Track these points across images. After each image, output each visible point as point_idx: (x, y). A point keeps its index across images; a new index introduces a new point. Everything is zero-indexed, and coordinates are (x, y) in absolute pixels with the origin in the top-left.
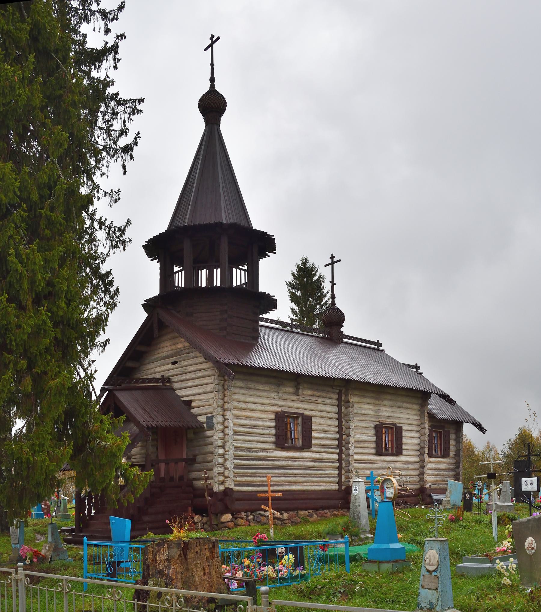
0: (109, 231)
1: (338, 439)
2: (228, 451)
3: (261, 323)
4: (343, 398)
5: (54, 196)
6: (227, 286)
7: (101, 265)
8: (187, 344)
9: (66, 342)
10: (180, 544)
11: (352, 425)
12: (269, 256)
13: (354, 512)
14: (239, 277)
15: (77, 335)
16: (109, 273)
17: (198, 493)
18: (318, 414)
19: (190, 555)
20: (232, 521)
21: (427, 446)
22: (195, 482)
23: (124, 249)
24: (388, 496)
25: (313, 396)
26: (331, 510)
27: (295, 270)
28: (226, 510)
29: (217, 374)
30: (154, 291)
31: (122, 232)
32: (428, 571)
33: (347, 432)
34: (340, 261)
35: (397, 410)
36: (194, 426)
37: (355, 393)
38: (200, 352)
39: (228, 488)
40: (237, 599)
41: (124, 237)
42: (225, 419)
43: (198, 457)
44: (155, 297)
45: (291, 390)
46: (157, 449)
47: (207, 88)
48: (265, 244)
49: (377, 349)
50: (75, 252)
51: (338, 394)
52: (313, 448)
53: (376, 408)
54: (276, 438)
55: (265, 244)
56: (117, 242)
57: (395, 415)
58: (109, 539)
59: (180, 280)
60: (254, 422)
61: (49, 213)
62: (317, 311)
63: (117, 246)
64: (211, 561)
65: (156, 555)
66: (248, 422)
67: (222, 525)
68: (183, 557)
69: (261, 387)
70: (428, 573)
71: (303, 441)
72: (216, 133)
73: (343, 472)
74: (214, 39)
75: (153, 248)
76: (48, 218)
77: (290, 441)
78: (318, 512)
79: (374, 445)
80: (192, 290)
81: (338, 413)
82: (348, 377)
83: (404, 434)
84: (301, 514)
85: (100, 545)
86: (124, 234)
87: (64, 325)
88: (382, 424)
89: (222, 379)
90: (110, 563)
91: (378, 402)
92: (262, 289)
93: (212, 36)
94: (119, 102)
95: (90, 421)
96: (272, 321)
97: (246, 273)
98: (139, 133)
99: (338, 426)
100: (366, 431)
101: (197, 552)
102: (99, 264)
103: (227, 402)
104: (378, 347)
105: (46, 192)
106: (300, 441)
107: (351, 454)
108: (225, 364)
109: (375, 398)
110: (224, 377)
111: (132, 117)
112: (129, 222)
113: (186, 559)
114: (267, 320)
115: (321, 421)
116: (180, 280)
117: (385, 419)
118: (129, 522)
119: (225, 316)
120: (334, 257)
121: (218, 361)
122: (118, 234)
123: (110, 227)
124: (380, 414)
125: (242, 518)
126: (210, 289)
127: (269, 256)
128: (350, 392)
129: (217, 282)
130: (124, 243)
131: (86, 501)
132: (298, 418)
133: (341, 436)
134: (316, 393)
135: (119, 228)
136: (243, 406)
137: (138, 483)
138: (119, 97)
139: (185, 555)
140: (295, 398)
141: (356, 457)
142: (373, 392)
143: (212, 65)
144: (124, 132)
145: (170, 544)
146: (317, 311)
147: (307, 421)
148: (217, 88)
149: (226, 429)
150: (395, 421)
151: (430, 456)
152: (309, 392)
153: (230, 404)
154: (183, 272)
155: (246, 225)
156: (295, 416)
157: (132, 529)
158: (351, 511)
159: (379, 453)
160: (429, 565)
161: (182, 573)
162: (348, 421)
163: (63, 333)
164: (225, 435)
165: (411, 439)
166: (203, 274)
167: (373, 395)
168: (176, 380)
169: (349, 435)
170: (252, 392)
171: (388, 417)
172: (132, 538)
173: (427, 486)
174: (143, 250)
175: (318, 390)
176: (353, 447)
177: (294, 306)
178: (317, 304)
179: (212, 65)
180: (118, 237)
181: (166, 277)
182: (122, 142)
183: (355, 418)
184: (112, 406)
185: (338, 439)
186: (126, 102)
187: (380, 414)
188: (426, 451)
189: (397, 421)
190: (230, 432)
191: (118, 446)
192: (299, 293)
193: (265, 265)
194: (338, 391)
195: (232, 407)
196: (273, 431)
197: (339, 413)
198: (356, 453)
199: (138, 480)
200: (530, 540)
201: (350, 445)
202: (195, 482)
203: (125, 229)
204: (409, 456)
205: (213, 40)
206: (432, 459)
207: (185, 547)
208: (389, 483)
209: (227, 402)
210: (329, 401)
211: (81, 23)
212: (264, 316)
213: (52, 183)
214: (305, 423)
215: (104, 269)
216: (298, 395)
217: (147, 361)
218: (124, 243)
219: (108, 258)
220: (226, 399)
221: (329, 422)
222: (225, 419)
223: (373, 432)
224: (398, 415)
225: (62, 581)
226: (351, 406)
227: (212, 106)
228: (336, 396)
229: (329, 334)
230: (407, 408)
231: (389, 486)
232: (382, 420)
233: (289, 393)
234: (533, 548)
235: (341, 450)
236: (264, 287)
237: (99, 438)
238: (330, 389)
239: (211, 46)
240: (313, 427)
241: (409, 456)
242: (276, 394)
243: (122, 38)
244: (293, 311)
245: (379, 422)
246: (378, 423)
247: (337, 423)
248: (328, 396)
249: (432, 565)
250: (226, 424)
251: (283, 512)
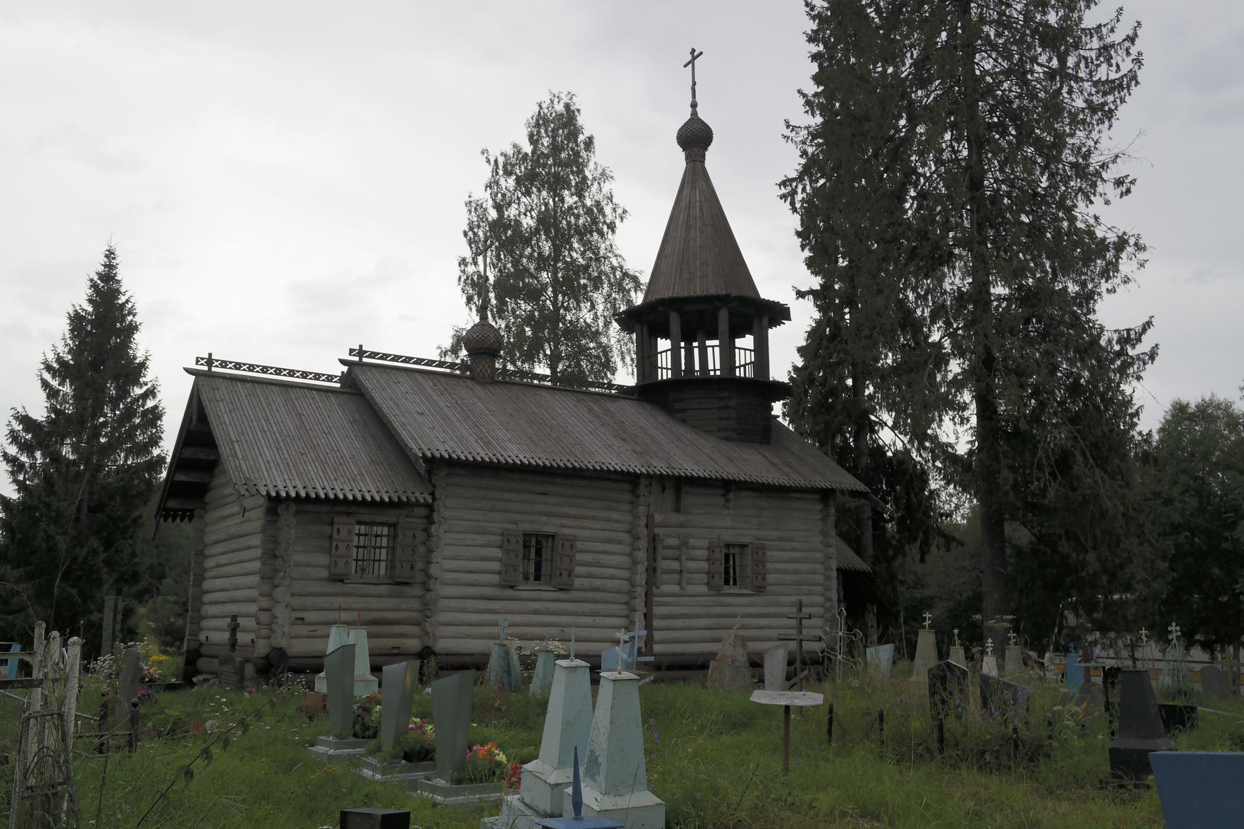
40: (703, 654)
77: (120, 608)
93: (693, 51)
143: (694, 84)
168: (617, 607)
181: (820, 66)
205: (695, 55)
211: (813, 18)
227: (695, 139)
239: (692, 62)
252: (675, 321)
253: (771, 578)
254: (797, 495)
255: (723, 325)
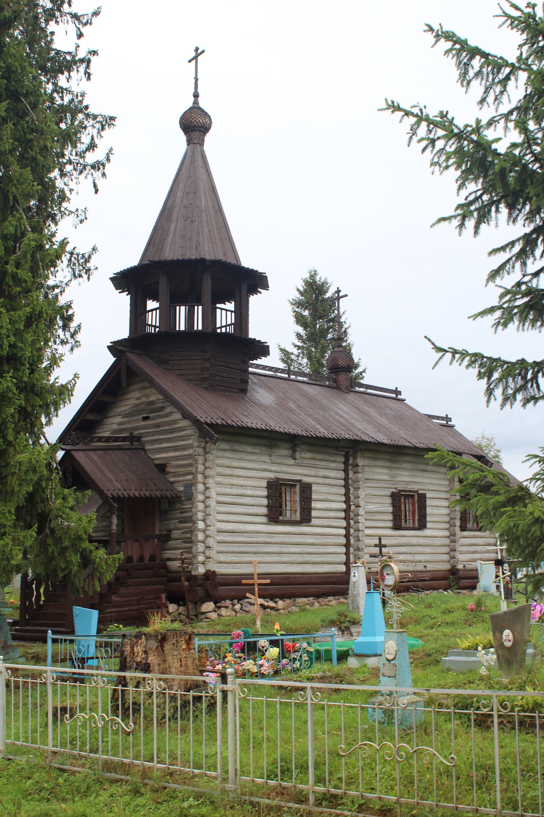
0: (71, 258)
1: (345, 511)
2: (210, 526)
3: (250, 369)
4: (351, 462)
5: (19, 250)
6: (210, 330)
7: (59, 296)
8: (160, 397)
9: (29, 409)
10: (157, 636)
11: (362, 493)
12: (261, 293)
13: (353, 601)
14: (225, 316)
15: (41, 403)
16: (69, 306)
17: (174, 578)
18: (320, 480)
19: (168, 647)
20: (215, 611)
21: (459, 517)
22: (169, 563)
23: (89, 278)
24: (389, 583)
25: (314, 459)
26: (337, 597)
27: (301, 286)
28: (208, 598)
29: (197, 434)
30: (123, 332)
31: (86, 259)
32: (388, 660)
33: (356, 501)
34: (346, 296)
35: (420, 474)
36: (169, 496)
37: (365, 455)
38: (177, 408)
39: (210, 571)
41: (88, 265)
42: (207, 488)
43: (173, 532)
44: (124, 340)
45: (287, 452)
46: (123, 521)
47: (190, 104)
48: (256, 281)
49: (396, 399)
50: (42, 312)
51: (345, 456)
52: (314, 522)
53: (392, 472)
54: (268, 510)
55: (256, 281)
56: (80, 271)
57: (417, 480)
58: (72, 632)
59: (153, 319)
60: (241, 491)
61: (15, 270)
62: (330, 336)
63: (80, 276)
64: (187, 653)
65: (133, 647)
66: (234, 491)
67: (203, 617)
68: (160, 649)
69: (249, 449)
70: (387, 662)
71: (301, 514)
72: (200, 163)
73: (351, 550)
74: (199, 51)
75: (123, 280)
76: (14, 277)
78: (320, 600)
79: (390, 517)
80: (168, 335)
81: (344, 480)
82: (355, 437)
83: (428, 502)
84: (299, 603)
85: (66, 640)
86: (89, 262)
87: (27, 391)
88: (401, 491)
89: (204, 440)
90: (78, 659)
91: (395, 465)
92: (251, 335)
93: (197, 49)
94: (88, 116)
95: (51, 497)
96: (264, 368)
97: (233, 314)
98: (111, 149)
99: (345, 495)
100: (380, 501)
101: (174, 644)
102: (57, 296)
103: (209, 468)
104: (397, 396)
105: (11, 243)
106: (298, 513)
107: (361, 529)
108: (206, 423)
109: (392, 461)
110: (205, 438)
111: (102, 133)
112: (94, 249)
113: (163, 651)
114: (258, 366)
115: (324, 489)
116: (153, 319)
117: (404, 486)
118: (95, 614)
119: (208, 365)
120: (340, 291)
121: (198, 421)
122: (81, 261)
123: (72, 254)
124: (398, 479)
125: (226, 607)
126: (190, 334)
127: (261, 293)
128: (359, 454)
129: (199, 325)
130: (88, 271)
131: (34, 586)
132: (295, 486)
133: (349, 506)
134: (317, 456)
135: (83, 254)
136: (228, 471)
137: (105, 568)
138: (89, 110)
139: (162, 647)
140: (292, 462)
141: (367, 532)
142: (388, 453)
143: (196, 79)
144: (92, 146)
145: (148, 636)
146: (330, 336)
147: (306, 490)
148: (202, 104)
149: (207, 500)
150: (415, 487)
151: (463, 528)
152: (309, 455)
153: (213, 470)
154: (158, 311)
155: (233, 262)
156: (291, 484)
157: (100, 621)
158: (350, 601)
159: (397, 526)
160: (388, 654)
161: (159, 665)
162: (357, 489)
163: (26, 400)
164: (206, 507)
165: (438, 509)
166: (182, 311)
167: (388, 457)
169: (358, 506)
170: (238, 455)
171: (407, 483)
172: (99, 631)
173: (460, 567)
174: (110, 282)
175: (318, 452)
176: (363, 520)
177: (300, 330)
178: (329, 328)
179: (196, 79)
180: (82, 266)
181: (138, 313)
182: (91, 158)
183: (366, 485)
184: (73, 475)
185: (345, 511)
186: (95, 117)
187: (398, 479)
188: (458, 523)
189: (420, 487)
190: (212, 503)
191: (84, 528)
192: (306, 313)
193: (256, 302)
194: (344, 453)
195: (215, 473)
196: (265, 502)
197: (346, 479)
198: (367, 527)
199: (106, 563)
200: (507, 632)
201: (360, 518)
202: (169, 563)
203: (90, 257)
204: (436, 529)
205: (198, 53)
206: (465, 533)
207: (162, 639)
208: (389, 569)
209: (209, 468)
210: (333, 465)
212: (255, 362)
213: (19, 234)
214: (303, 492)
215: (62, 301)
216: (295, 459)
217: (111, 414)
218: (88, 271)
219: (68, 288)
220: (207, 464)
221: (334, 490)
222: (207, 488)
223: (389, 500)
224: (420, 480)
225: (46, 672)
226: (360, 471)
227: (195, 125)
228: (343, 459)
229: (335, 381)
230: (432, 471)
231: (389, 573)
232: (400, 487)
233: (284, 456)
234: (510, 641)
235: (349, 524)
236: (255, 332)
237: (62, 517)
238: (334, 451)
239: (196, 58)
240: (314, 496)
241: (436, 529)
242: (268, 457)
243: (94, 55)
244: (299, 336)
245: (396, 488)
246: (395, 490)
247: (343, 491)
248: (332, 459)
249: (391, 654)
250: (208, 493)
251: (277, 600)
252: (163, 287)
253: (314, 513)
254: (409, 452)
255: (207, 296)
